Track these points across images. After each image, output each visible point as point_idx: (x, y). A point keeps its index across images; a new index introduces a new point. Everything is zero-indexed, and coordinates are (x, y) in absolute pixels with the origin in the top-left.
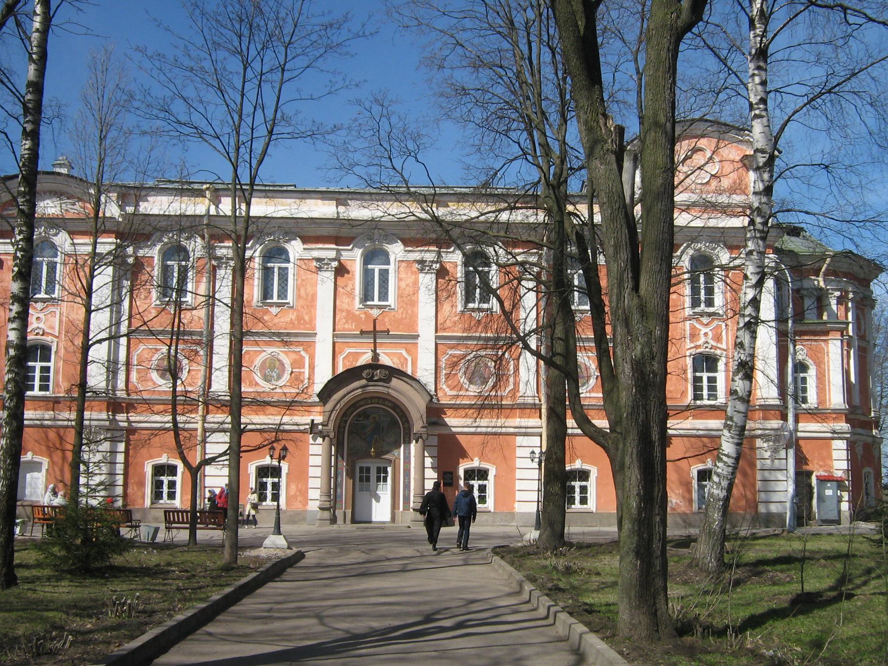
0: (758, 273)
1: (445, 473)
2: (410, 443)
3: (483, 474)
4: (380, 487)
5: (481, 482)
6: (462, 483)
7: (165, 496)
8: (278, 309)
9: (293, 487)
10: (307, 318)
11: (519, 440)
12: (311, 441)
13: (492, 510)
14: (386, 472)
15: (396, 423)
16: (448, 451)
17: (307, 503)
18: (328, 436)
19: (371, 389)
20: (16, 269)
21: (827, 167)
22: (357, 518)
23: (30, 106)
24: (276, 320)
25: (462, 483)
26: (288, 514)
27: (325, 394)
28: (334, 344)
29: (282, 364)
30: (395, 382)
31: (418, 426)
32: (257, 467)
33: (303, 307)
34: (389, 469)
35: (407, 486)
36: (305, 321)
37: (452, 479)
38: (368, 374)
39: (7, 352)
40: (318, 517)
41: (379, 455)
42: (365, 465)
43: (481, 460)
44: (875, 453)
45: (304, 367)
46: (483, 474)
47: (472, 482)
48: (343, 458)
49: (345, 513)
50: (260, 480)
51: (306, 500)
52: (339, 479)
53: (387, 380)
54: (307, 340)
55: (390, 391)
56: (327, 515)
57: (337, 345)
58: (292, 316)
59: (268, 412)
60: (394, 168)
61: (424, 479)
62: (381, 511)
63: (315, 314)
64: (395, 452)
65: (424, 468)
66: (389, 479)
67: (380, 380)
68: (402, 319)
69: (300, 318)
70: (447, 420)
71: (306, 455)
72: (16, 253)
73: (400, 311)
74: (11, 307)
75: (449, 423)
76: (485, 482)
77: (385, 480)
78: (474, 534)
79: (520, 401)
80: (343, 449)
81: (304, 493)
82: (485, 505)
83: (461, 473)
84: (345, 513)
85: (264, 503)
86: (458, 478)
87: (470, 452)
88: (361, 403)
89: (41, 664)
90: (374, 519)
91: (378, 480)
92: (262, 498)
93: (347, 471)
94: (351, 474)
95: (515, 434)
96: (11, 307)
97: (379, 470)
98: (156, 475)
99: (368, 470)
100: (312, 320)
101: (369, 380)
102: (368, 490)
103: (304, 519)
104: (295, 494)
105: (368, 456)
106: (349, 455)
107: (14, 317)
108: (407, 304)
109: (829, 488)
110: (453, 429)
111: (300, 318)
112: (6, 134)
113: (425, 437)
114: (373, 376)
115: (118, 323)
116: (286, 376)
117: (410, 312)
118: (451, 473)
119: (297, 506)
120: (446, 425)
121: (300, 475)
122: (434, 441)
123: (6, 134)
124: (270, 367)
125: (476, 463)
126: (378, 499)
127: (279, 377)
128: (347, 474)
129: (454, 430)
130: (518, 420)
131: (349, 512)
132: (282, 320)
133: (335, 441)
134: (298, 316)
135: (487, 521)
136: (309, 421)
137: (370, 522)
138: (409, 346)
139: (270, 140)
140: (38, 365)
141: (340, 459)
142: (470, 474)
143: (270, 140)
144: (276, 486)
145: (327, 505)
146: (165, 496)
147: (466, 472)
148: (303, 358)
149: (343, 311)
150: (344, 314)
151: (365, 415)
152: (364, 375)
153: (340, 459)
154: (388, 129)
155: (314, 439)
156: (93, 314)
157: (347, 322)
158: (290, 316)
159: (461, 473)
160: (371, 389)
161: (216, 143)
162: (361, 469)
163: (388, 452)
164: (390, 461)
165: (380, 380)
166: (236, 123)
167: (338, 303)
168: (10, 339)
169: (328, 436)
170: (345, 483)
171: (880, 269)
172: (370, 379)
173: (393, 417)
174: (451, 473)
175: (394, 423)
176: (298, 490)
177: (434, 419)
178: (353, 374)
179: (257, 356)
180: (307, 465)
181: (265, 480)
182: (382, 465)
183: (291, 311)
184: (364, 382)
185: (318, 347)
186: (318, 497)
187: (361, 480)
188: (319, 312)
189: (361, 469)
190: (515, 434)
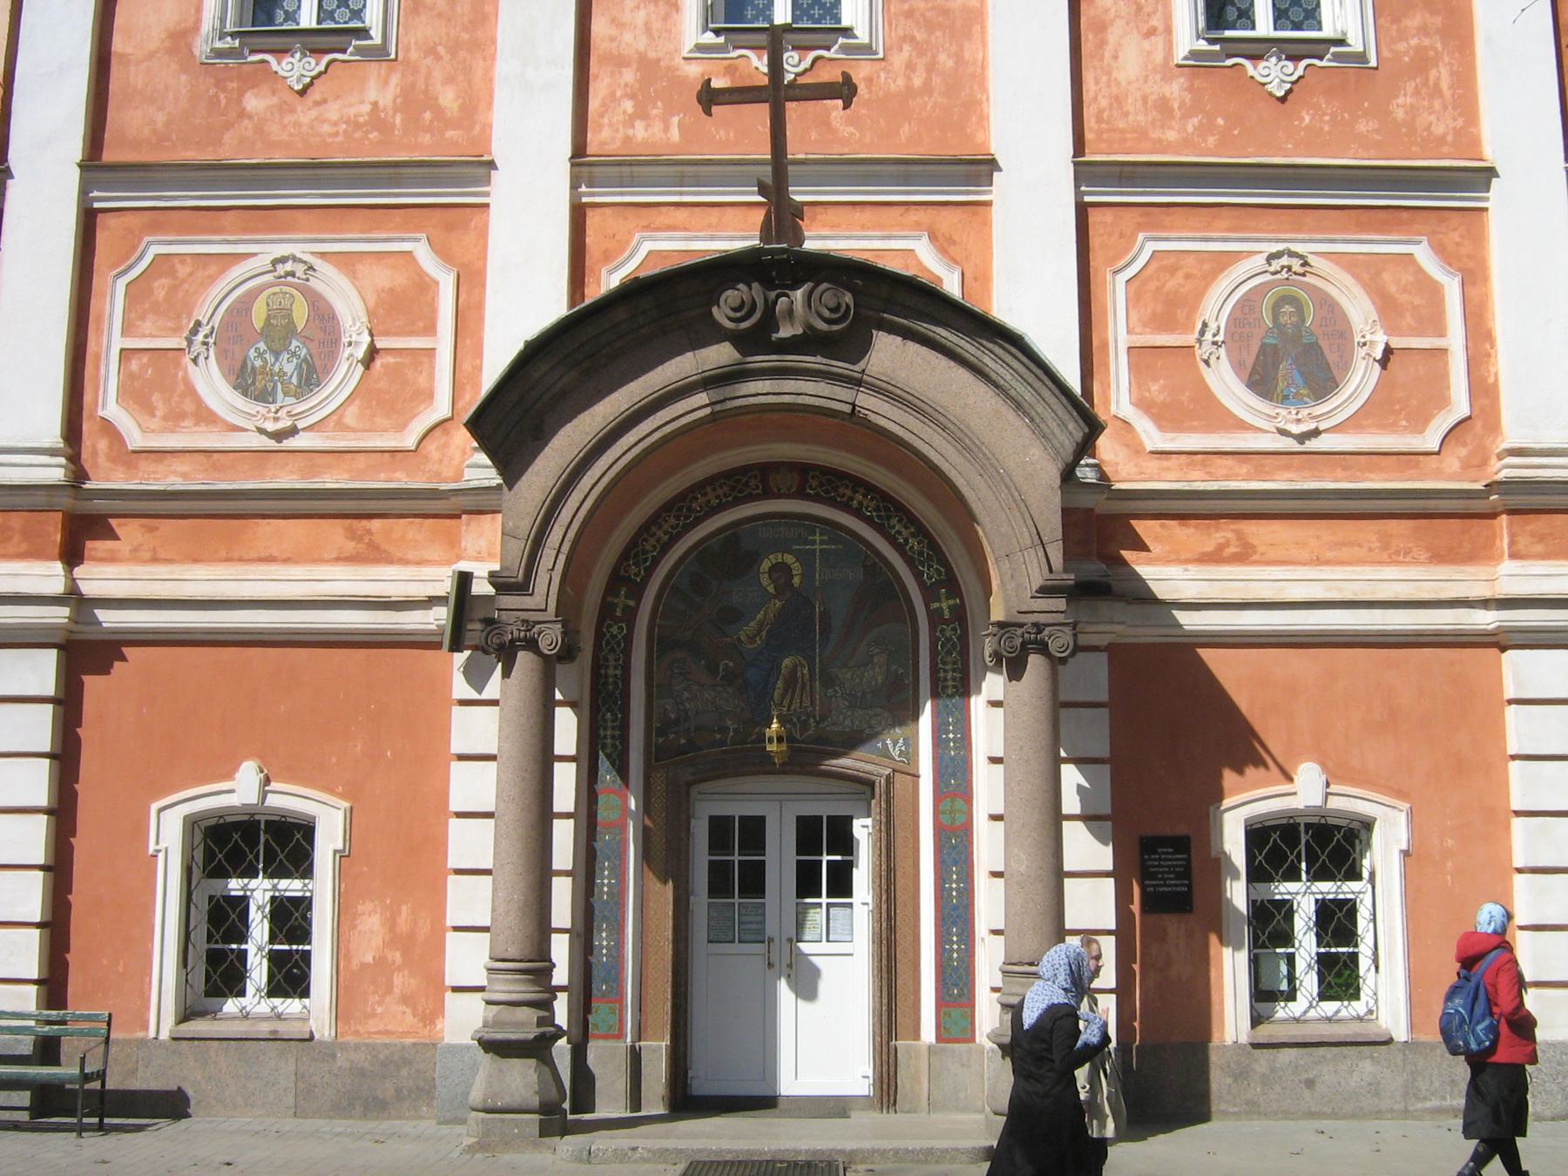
1: (1149, 845)
2: (965, 689)
3: (1333, 846)
4: (816, 918)
5: (1326, 888)
6: (1237, 893)
7: (258, 971)
8: (314, 65)
9: (371, 923)
10: (448, 99)
11: (1522, 670)
12: (461, 688)
13: (1401, 1034)
14: (843, 841)
16: (1158, 731)
17: (439, 1010)
18: (532, 645)
19: (758, 390)
22: (703, 1083)
24: (305, 114)
25: (1237, 893)
26: (342, 1060)
27: (512, 418)
28: (579, 214)
29: (324, 315)
30: (889, 354)
31: (1016, 574)
32: (191, 823)
33: (431, 51)
34: (862, 830)
35: (956, 916)
36: (439, 112)
37: (1186, 873)
38: (744, 309)
40: (476, 1095)
41: (808, 755)
43: (1335, 774)
45: (430, 329)
46: (1333, 846)
47: (1284, 889)
48: (622, 771)
49: (635, 1057)
50: (215, 886)
51: (433, 990)
52: (605, 881)
53: (843, 343)
54: (442, 181)
55: (866, 400)
56: (521, 1079)
57: (593, 220)
58: (376, 91)
59: (655, 885)
61: (1059, 875)
62: (822, 1040)
63: (489, 81)
64: (892, 741)
65: (1057, 817)
66: (862, 878)
67: (809, 342)
68: (910, 92)
69: (415, 102)
70: (1145, 571)
71: (432, 757)
73: (898, 60)
75: (1161, 591)
76: (1348, 889)
77: (841, 885)
79: (1505, 470)
80: (625, 727)
81: (423, 953)
82: (1358, 1007)
83: (1234, 844)
84: (635, 1057)
85: (231, 1006)
86: (1218, 866)
87: (1272, 735)
90: (789, 1084)
91: (807, 884)
92: (223, 975)
93: (646, 838)
94: (665, 856)
95: (1499, 641)
97: (809, 834)
99: (754, 831)
100: (476, 105)
101: (748, 342)
102: (759, 937)
103: (425, 1091)
104: (380, 961)
105: (761, 764)
106: (656, 756)
108: (930, 27)
110: (1183, 618)
111: (415, 102)
113: (1059, 642)
114: (770, 321)
116: (344, 376)
117: (945, 61)
118: (1181, 844)
119: (390, 1022)
120: (1143, 597)
121: (404, 856)
122: (1093, 677)
124: (267, 332)
125: (1306, 790)
126: (807, 984)
127: (311, 378)
128: (646, 855)
129: (1190, 621)
130: (1508, 566)
131: (657, 1050)
132: (333, 111)
133: (575, 677)
134: (407, 92)
135: (1375, 1088)
136: (446, 587)
137: (766, 1102)
138: (948, 221)
141: (607, 776)
142: (1277, 847)
144: (291, 919)
145: (525, 1024)
146: (258, 971)
147: (1256, 835)
148: (426, 286)
149: (620, 62)
150: (629, 76)
151: (731, 557)
152: (721, 315)
153: (607, 776)
155: (477, 677)
157: (641, 114)
158: (372, 94)
159: (1234, 844)
160: (758, 390)
162: (720, 827)
163: (852, 742)
164: (863, 787)
165: (809, 342)
167: (599, 26)
169: (532, 645)
170: (639, 905)
172: (755, 338)
173: (874, 564)
174: (1181, 844)
175: (881, 593)
176: (395, 939)
177: (1094, 569)
178: (664, 307)
179: (212, 279)
180: (439, 809)
181: (235, 885)
182: (824, 809)
183: (374, 70)
184: (721, 354)
185: (500, 224)
186: (481, 979)
187: (719, 883)
188: (505, 67)
189: (720, 827)
190: (1499, 641)
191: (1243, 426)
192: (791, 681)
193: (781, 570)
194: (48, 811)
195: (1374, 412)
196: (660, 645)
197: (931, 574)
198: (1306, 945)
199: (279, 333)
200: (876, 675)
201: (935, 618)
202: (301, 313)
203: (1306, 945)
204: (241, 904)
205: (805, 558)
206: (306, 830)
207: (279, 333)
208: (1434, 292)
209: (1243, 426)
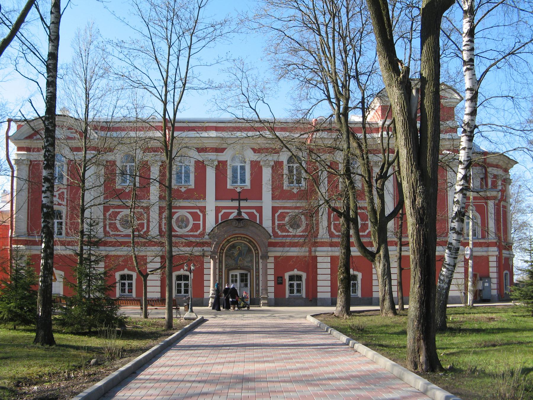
0: (467, 161)
1: (278, 277)
15: (251, 250)
20: (45, 162)
21: (512, 98)
23: (50, 67)
39: (42, 210)
42: (234, 274)
44: (510, 263)
60: (251, 107)
72: (45, 153)
74: (43, 184)
78: (452, 297)
88: (231, 240)
89: (269, 393)
96: (43, 184)
98: (121, 280)
99: (236, 276)
107: (46, 190)
109: (487, 282)
112: (37, 83)
115: (283, 129)
118: (281, 277)
123: (37, 83)
139: (184, 90)
140: (56, 221)
143: (184, 90)
154: (247, 86)
156: (86, 192)
161: (154, 91)
162: (232, 275)
166: (165, 79)
168: (44, 202)
171: (516, 163)
173: (249, 248)
174: (281, 277)
175: (250, 250)
189: (232, 275)
191: (177, 232)
192: (240, 260)
193: (239, 248)
194: (497, 267)
195: (191, 230)
196: (226, 256)
197: (255, 249)
198: (295, 287)
199: (182, 221)
200: (249, 259)
201: (255, 253)
202: (185, 219)
203: (295, 287)
204: (181, 284)
205: (242, 247)
206: (132, 276)
207: (182, 221)
208: (334, 229)
209: (177, 232)
